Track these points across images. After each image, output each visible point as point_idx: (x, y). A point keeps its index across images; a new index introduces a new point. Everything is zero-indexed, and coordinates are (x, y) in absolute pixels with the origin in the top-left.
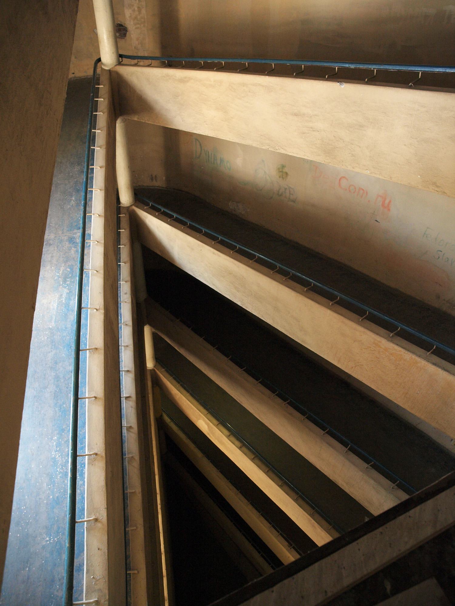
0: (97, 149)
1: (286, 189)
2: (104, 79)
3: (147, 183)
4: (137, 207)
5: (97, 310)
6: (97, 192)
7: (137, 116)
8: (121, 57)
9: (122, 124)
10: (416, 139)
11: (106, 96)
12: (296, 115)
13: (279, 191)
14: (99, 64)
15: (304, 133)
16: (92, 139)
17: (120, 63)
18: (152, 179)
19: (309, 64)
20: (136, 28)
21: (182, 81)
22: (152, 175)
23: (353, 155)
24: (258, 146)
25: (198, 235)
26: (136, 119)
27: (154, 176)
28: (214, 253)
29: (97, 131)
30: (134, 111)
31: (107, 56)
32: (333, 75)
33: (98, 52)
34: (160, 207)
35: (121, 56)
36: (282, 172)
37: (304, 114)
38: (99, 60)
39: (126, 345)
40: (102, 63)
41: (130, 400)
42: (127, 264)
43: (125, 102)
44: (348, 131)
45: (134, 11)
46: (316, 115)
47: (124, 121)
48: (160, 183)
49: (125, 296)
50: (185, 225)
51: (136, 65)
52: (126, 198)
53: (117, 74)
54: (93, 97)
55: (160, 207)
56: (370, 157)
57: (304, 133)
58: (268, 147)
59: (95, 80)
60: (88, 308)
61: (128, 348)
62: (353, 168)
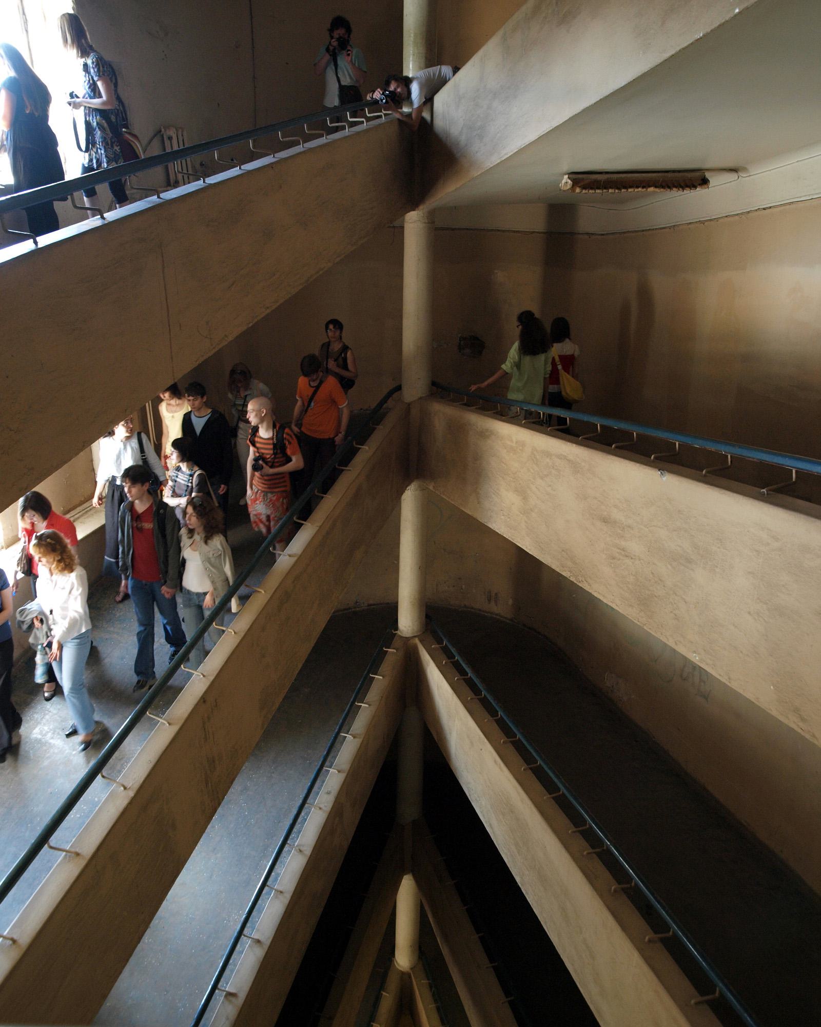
5: (125, 788)
10: (766, 604)
12: (605, 520)
18: (489, 600)
23: (677, 618)
25: (487, 718)
28: (495, 762)
34: (453, 650)
37: (615, 522)
39: (281, 889)
41: (230, 1002)
42: (356, 740)
44: (669, 566)
46: (629, 527)
47: (423, 489)
48: (502, 609)
49: (326, 796)
50: (476, 695)
55: (453, 650)
57: (614, 558)
60: (115, 781)
61: (281, 896)
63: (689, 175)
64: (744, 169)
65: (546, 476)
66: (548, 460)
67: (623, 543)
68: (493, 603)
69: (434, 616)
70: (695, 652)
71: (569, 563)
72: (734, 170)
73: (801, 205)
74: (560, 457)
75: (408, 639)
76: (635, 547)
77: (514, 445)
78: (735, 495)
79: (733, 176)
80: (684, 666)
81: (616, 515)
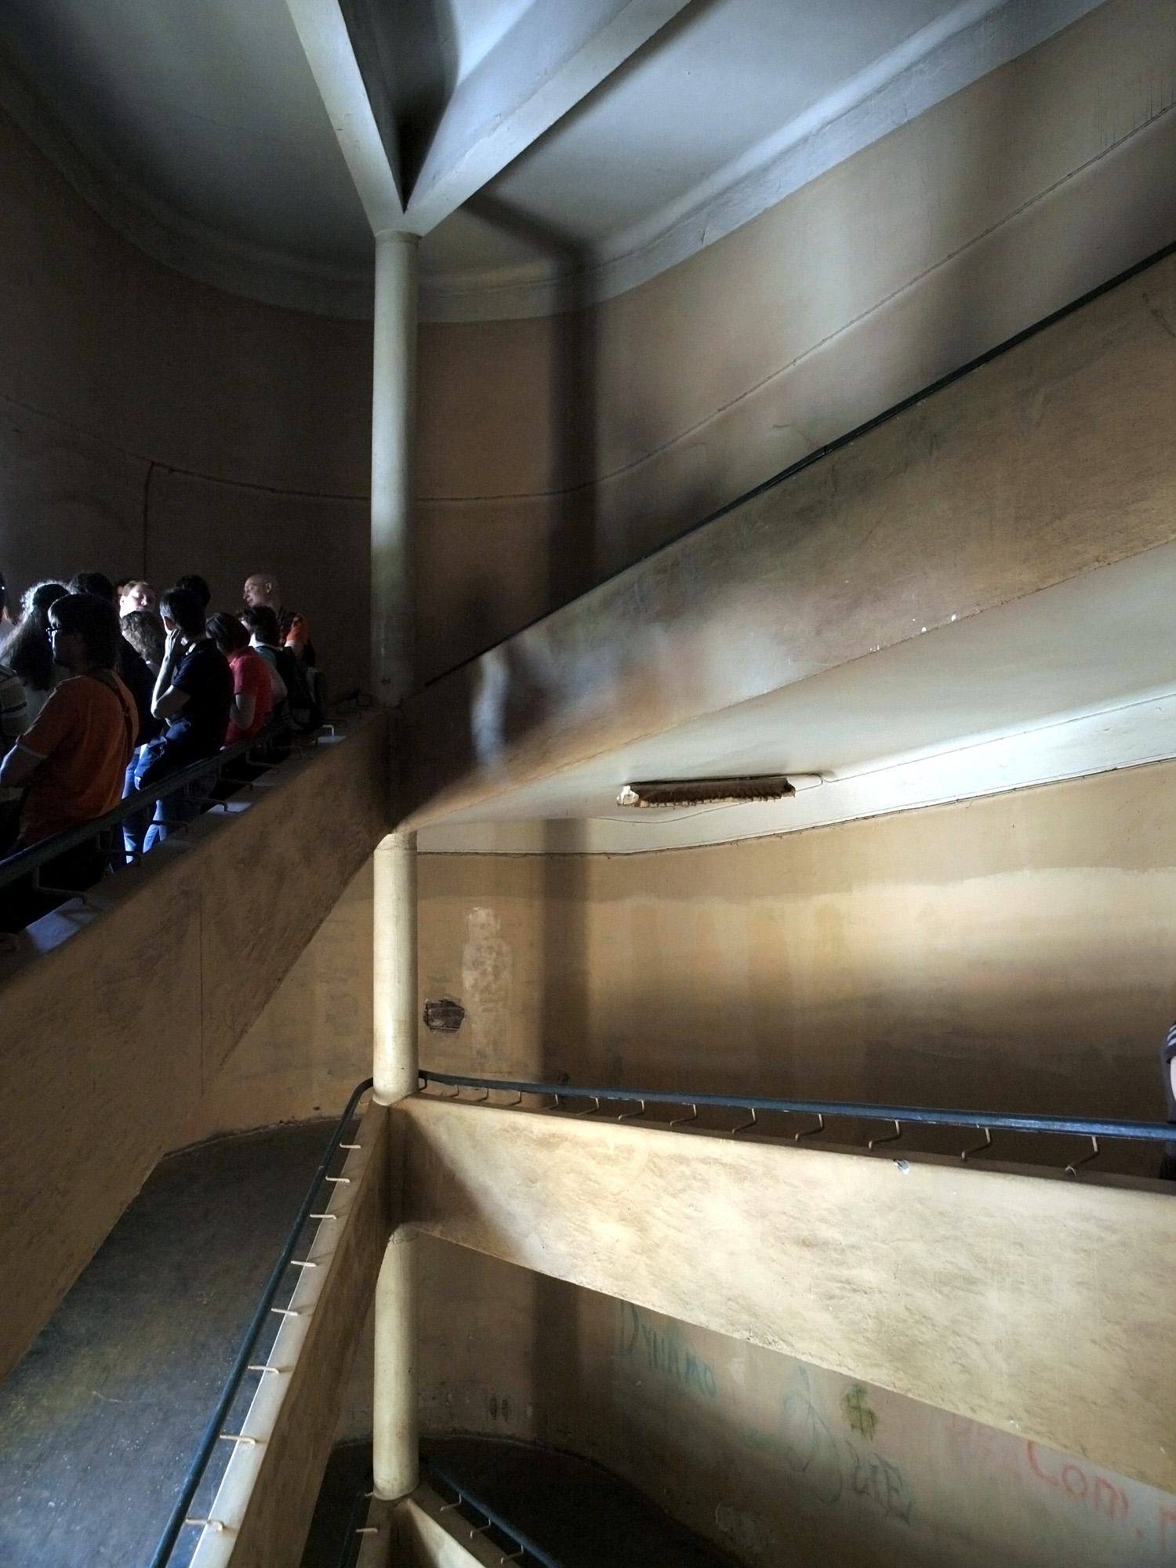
0: (290, 1314)
1: (874, 1469)
2: (369, 1131)
3: (479, 1422)
4: (419, 1503)
6: (245, 1447)
7: (440, 1227)
8: (421, 1080)
9: (403, 1245)
10: (1118, 1323)
11: (359, 1172)
12: (806, 1243)
13: (855, 1476)
14: (366, 1092)
15: (831, 1297)
16: (282, 1285)
17: (416, 1092)
18: (494, 1413)
19: (833, 1111)
20: (485, 1010)
21: (547, 1143)
22: (494, 1399)
23: (965, 1369)
24: (723, 1331)
26: (436, 1234)
27: (500, 1401)
29: (306, 1264)
30: (435, 1214)
31: (389, 1074)
32: (888, 1140)
33: (369, 1064)
34: (483, 1510)
35: (423, 1075)
36: (858, 1408)
37: (826, 1243)
38: (369, 1083)
40: (374, 1092)
43: (413, 1186)
45: (484, 973)
46: (853, 1247)
47: (412, 1238)
48: (516, 1426)
51: (452, 1099)
52: (389, 1471)
53: (407, 1116)
54: (323, 1174)
55: (483, 1510)
56: (1011, 1376)
57: (831, 1297)
58: (746, 1334)
59: (347, 1127)
62: (973, 1410)
63: (769, 781)
64: (829, 773)
65: (680, 1191)
66: (683, 1168)
67: (845, 1273)
68: (501, 1420)
69: (437, 1458)
70: (1010, 1418)
71: (745, 1318)
72: (816, 774)
73: (914, 813)
74: (705, 1161)
75: (393, 1503)
76: (867, 1275)
77: (611, 1152)
78: (1031, 1179)
79: (817, 781)
80: (858, 1468)
81: (825, 1232)
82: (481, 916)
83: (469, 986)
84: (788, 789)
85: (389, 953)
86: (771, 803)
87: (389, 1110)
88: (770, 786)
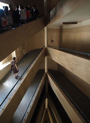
8: (48, 46)
12: (68, 61)
17: (48, 47)
31: (46, 46)
38: (44, 46)
43: (47, 53)
48: (56, 69)
52: (46, 71)
53: (47, 48)
69: (49, 70)
74: (63, 54)
76: (71, 64)
81: (69, 60)
82: (55, 34)
83: (54, 39)
84: (77, 23)
85: (46, 36)
86: (75, 24)
87: (46, 48)
88: (76, 23)
